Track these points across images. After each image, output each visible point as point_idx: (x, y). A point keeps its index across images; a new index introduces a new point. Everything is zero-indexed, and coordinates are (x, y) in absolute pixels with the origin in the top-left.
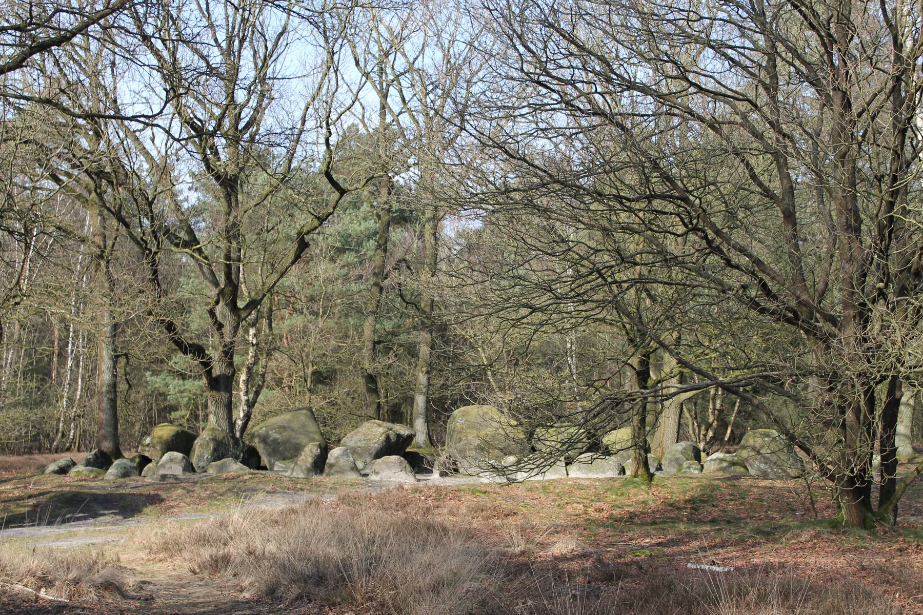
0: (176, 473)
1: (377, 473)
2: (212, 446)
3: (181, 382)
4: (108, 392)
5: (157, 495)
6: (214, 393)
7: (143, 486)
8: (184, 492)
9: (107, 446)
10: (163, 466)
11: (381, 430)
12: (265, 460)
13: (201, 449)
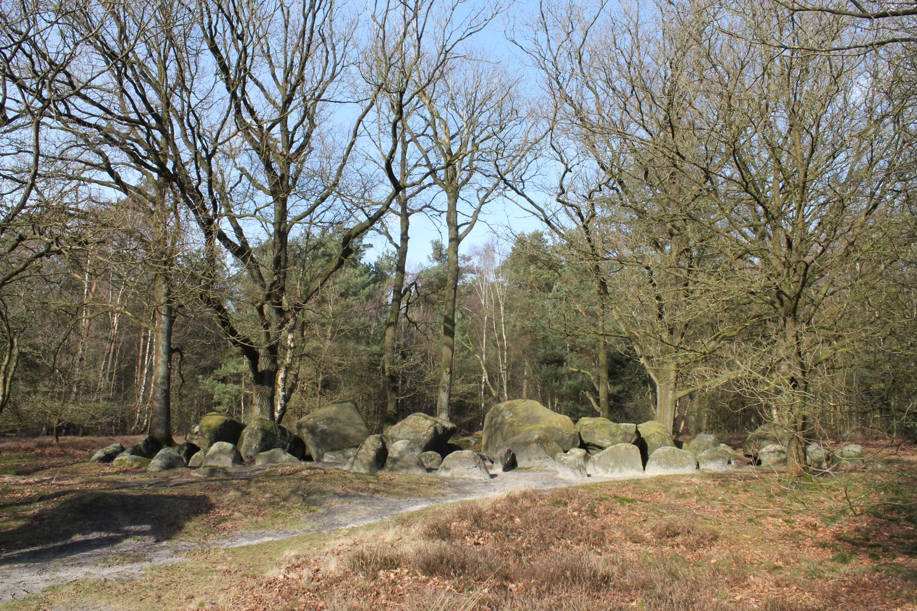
0: (225, 465)
1: (447, 469)
2: (260, 435)
3: (224, 385)
4: (162, 383)
5: (205, 497)
6: (259, 386)
7: (188, 482)
8: (238, 494)
9: (159, 432)
10: (212, 457)
11: (429, 422)
12: (312, 450)
13: (249, 441)
